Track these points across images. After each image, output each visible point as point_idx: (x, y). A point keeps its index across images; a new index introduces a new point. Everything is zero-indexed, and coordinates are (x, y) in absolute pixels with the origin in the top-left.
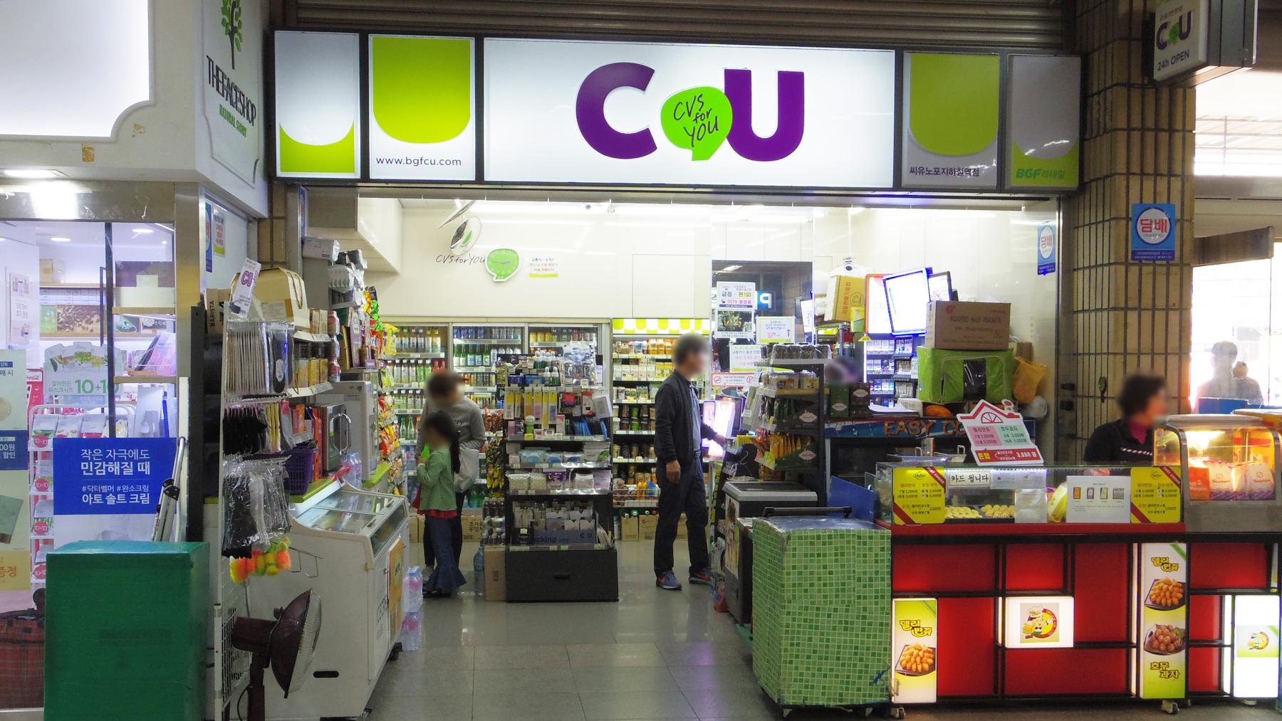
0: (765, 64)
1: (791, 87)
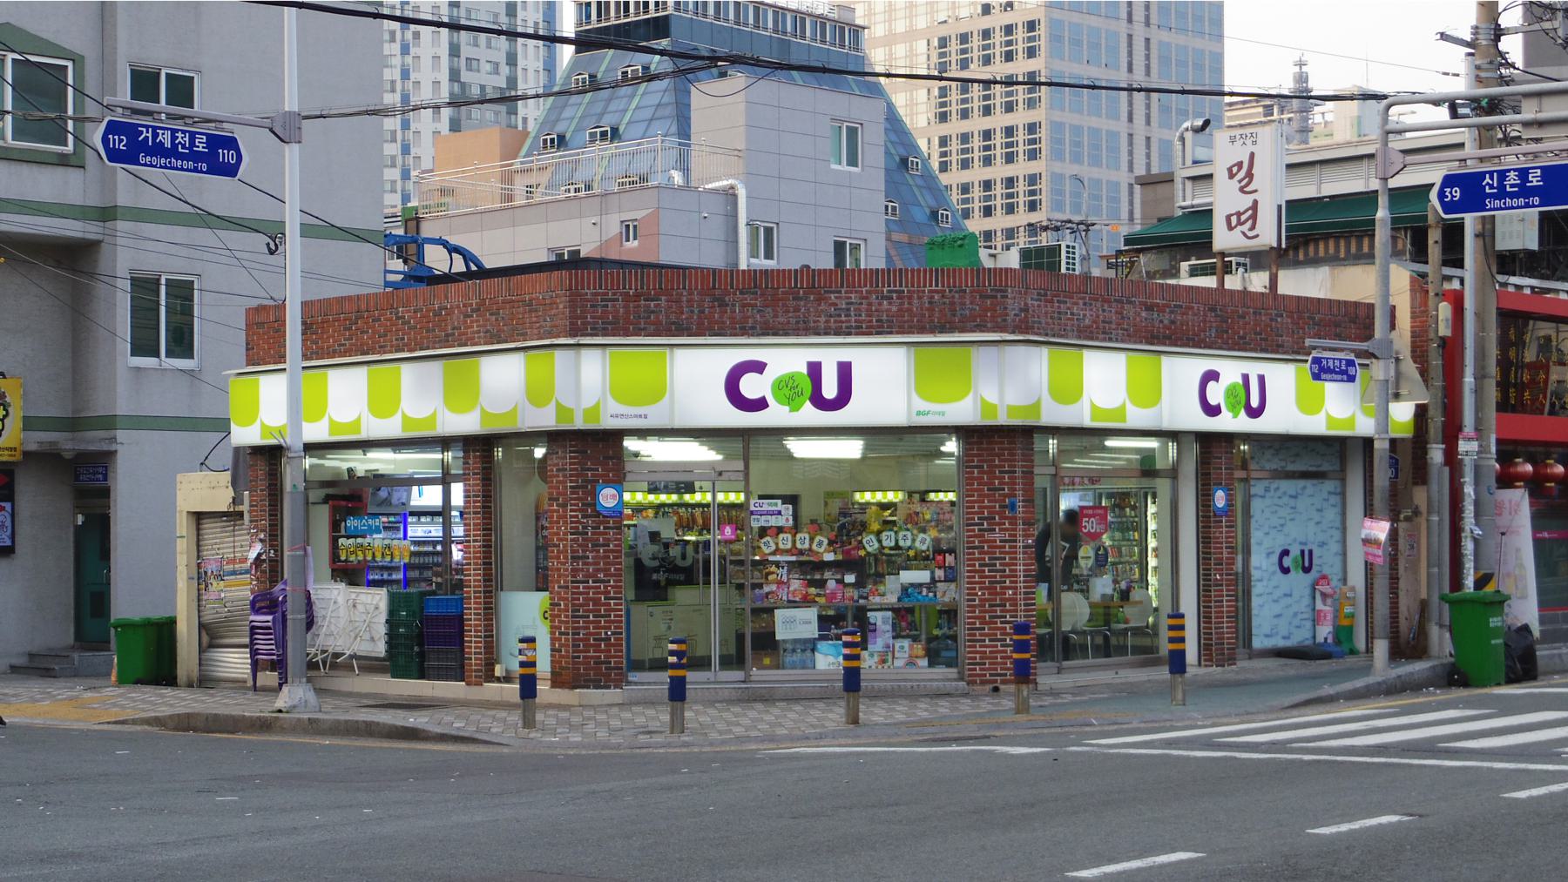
0: (829, 360)
1: (845, 371)
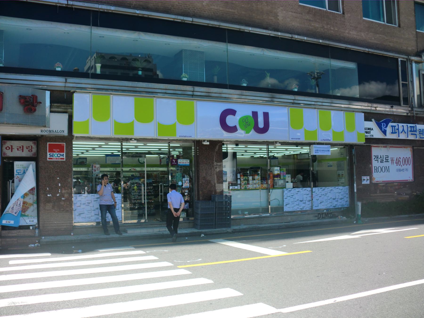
1: (266, 115)
